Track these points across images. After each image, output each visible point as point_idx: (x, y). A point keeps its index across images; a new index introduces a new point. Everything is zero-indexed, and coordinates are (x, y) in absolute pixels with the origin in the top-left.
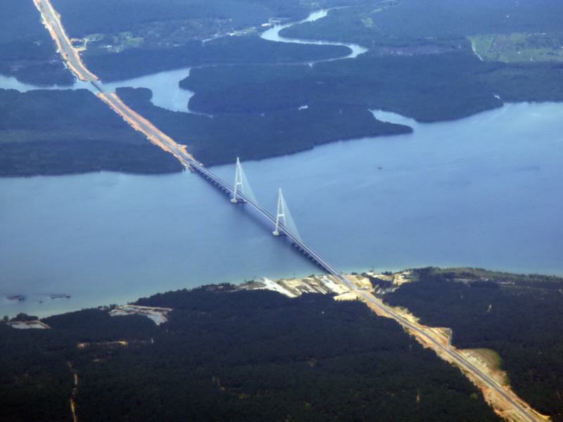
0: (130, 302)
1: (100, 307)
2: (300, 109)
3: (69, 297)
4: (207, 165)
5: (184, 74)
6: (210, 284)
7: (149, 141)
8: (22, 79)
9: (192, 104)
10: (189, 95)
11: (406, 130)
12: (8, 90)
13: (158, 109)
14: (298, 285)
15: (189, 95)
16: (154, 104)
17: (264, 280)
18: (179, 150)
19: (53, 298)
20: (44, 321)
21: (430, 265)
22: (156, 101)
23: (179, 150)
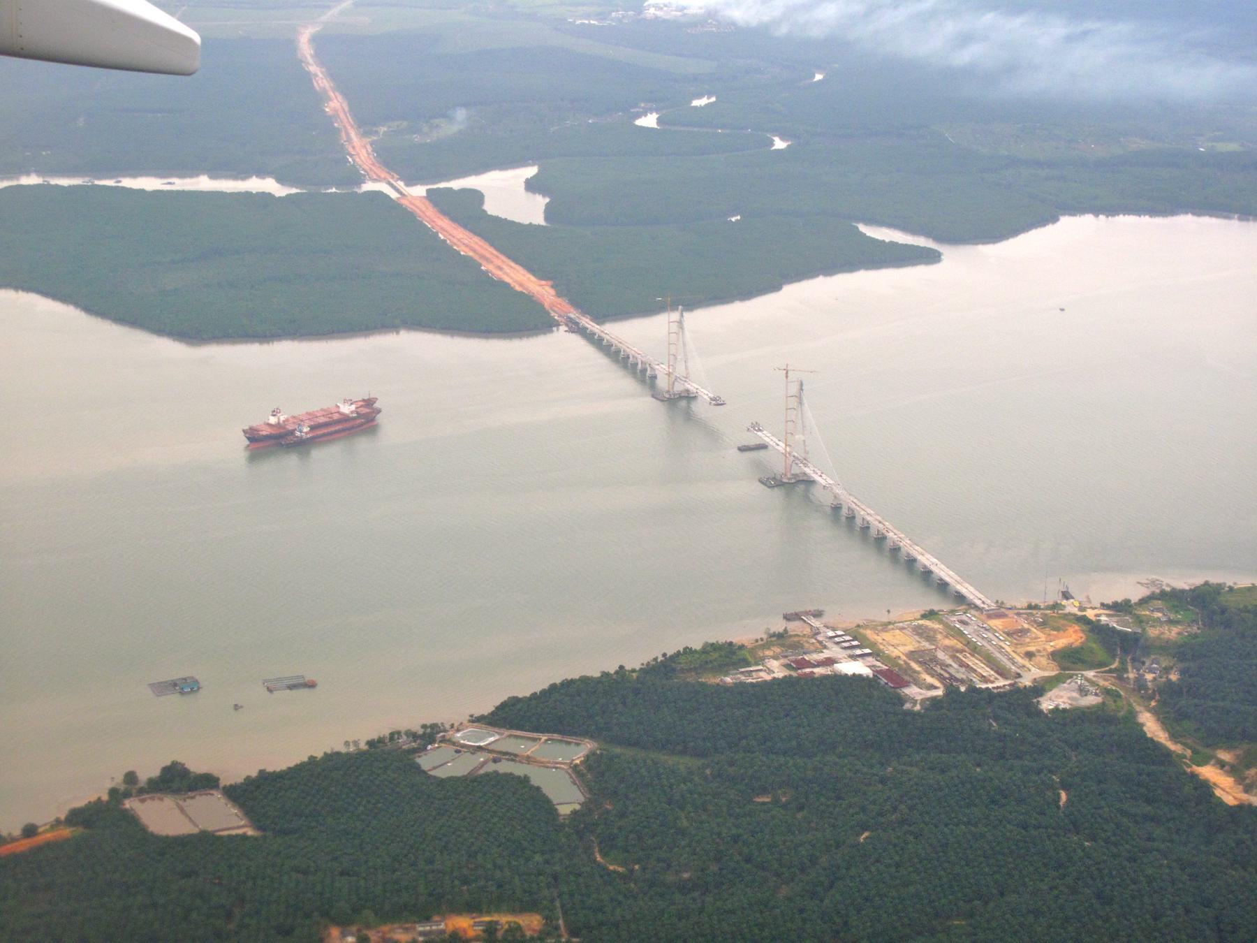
0: (477, 714)
1: (394, 735)
2: (713, 99)
3: (311, 685)
4: (600, 318)
5: (531, 171)
6: (558, 681)
7: (486, 273)
8: (281, 180)
9: (549, 212)
10: (541, 201)
11: (931, 257)
12: (257, 193)
13: (497, 220)
14: (910, 648)
15: (541, 201)
16: (489, 213)
17: (874, 675)
18: (543, 291)
19: (270, 690)
20: (237, 794)
21: (1215, 579)
22: (492, 207)
23: (543, 291)
